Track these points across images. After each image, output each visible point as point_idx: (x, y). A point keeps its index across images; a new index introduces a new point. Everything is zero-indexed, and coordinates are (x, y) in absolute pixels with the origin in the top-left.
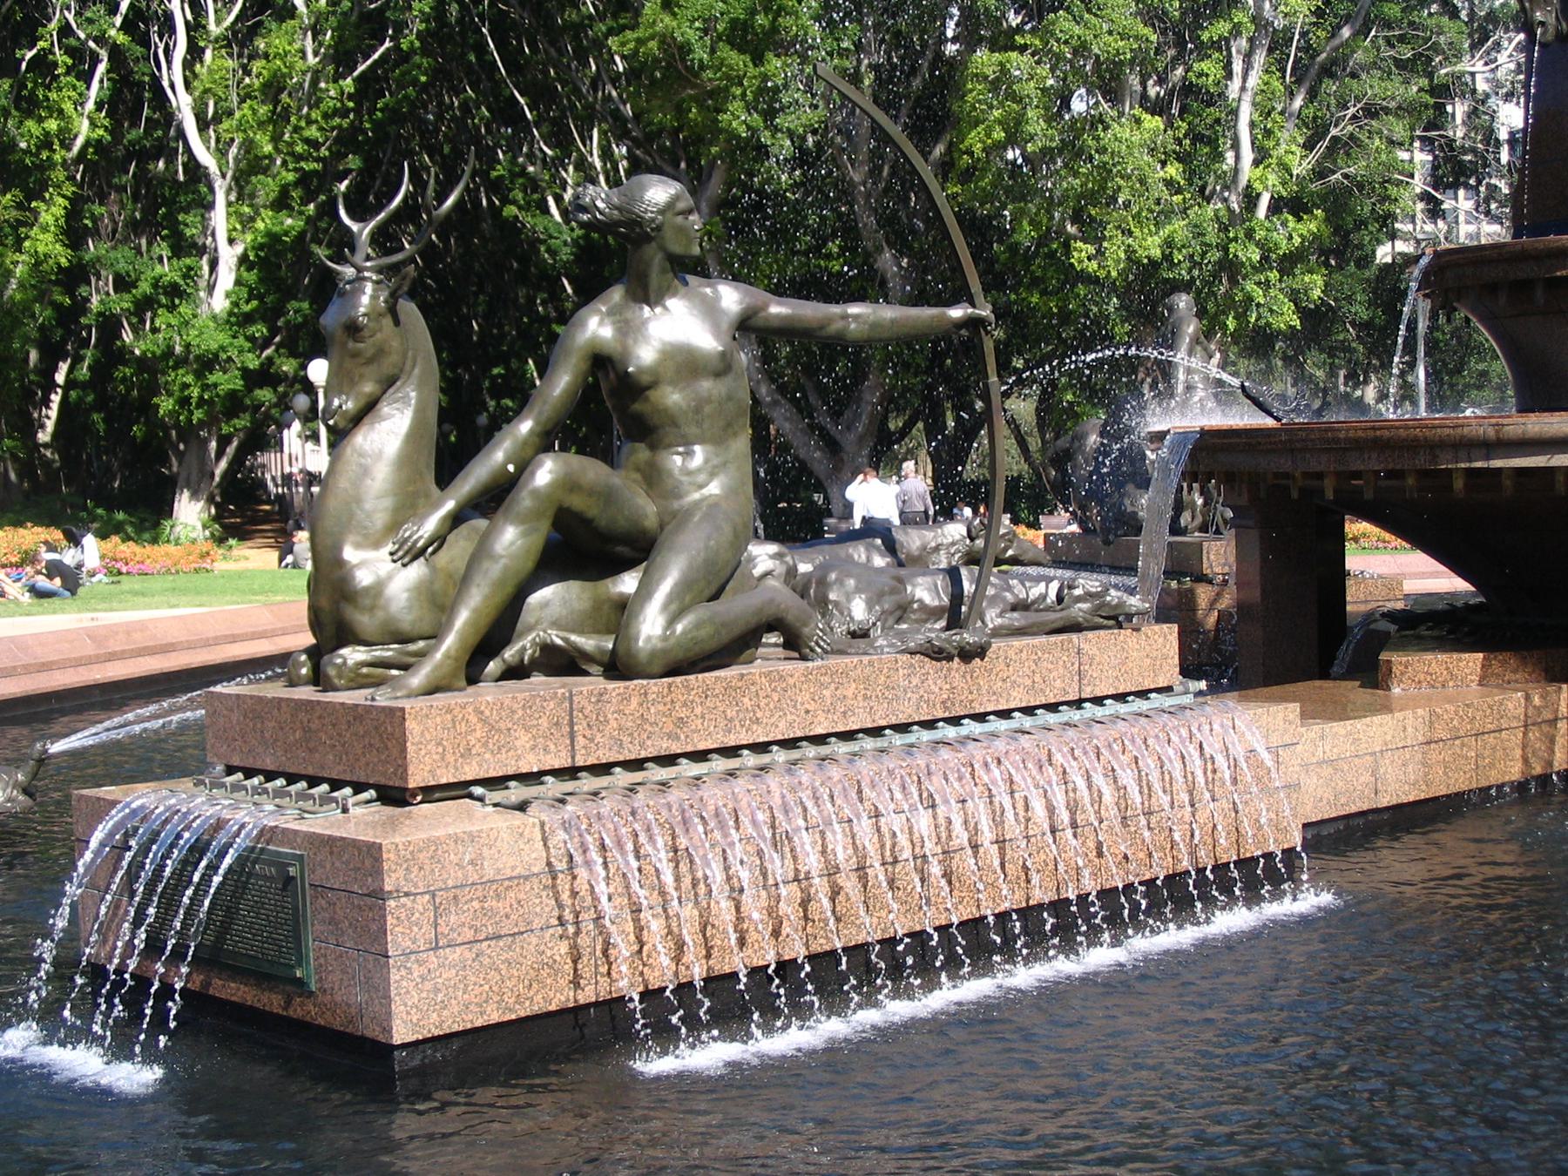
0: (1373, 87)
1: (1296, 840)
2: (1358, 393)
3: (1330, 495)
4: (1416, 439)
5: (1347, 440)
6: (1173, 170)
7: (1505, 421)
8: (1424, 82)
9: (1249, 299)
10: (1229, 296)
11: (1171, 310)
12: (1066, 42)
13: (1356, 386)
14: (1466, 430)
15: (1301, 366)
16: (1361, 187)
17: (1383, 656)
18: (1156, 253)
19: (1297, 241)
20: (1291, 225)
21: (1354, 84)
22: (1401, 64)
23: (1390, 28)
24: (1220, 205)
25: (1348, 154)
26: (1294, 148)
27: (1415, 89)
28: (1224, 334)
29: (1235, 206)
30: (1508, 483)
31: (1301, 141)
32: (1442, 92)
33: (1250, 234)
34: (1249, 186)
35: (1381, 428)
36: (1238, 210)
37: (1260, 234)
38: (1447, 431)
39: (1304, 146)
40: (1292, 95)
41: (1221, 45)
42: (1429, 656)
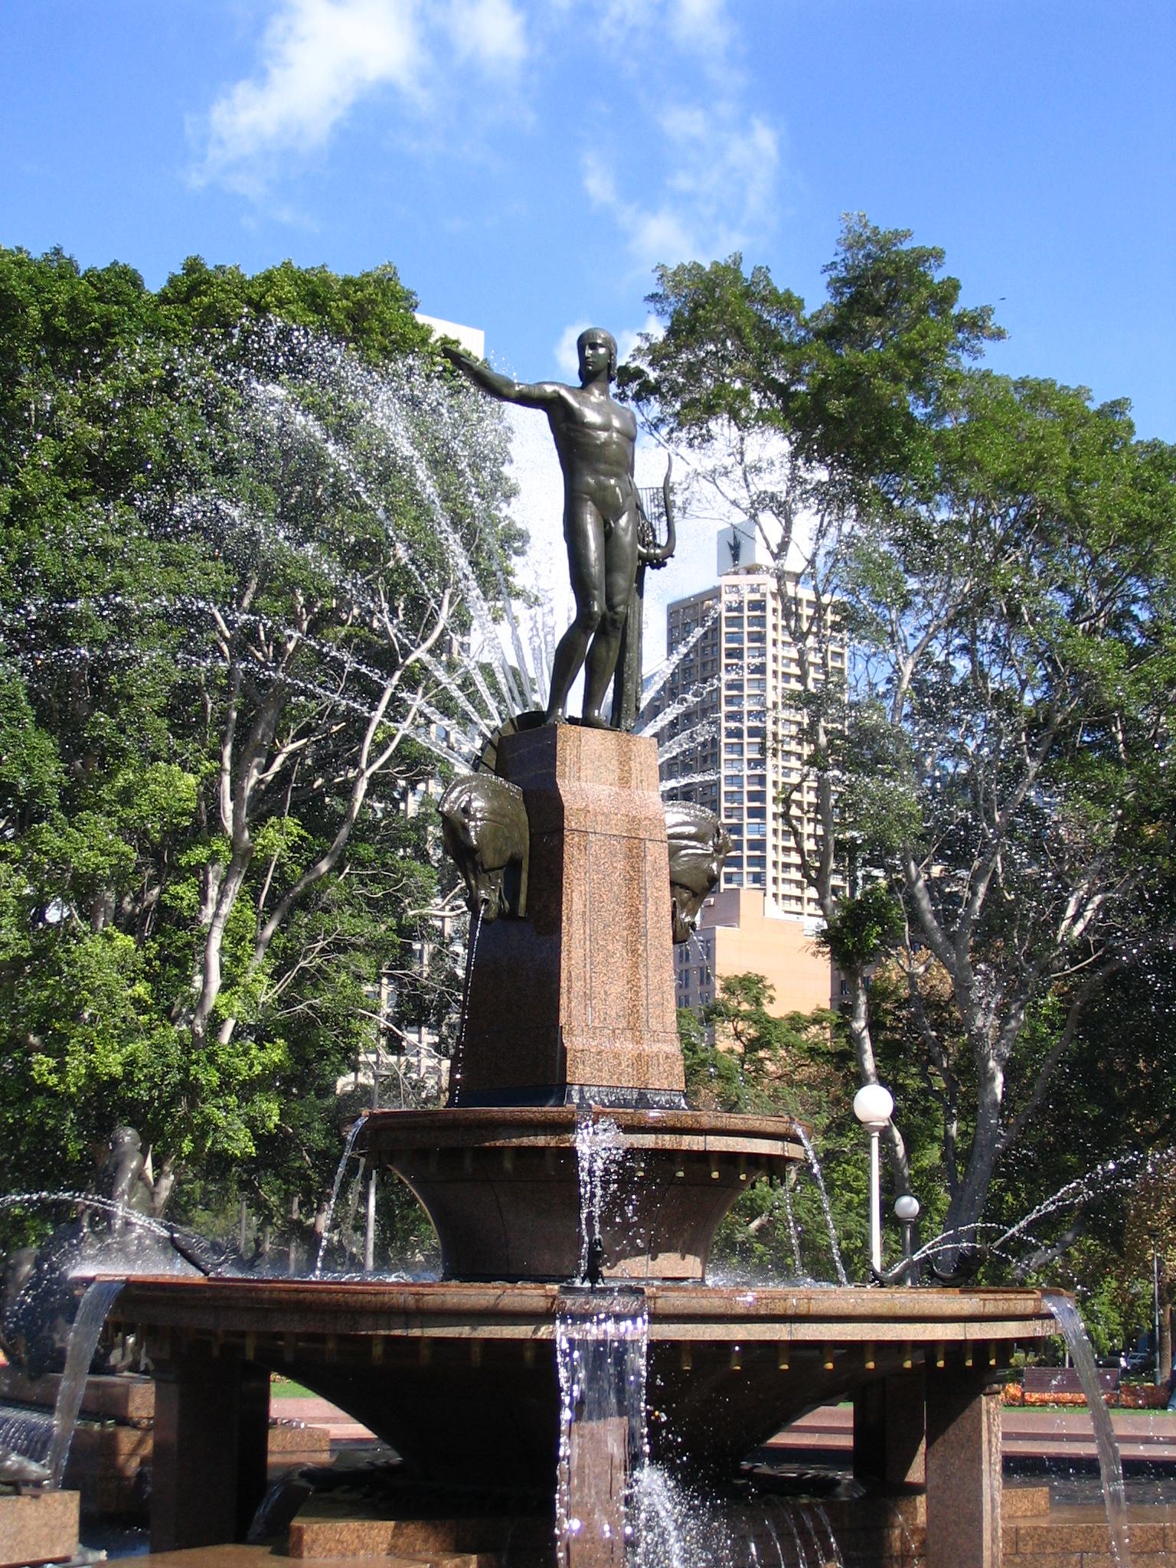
0: (344, 923)
1: (839, 1013)
2: (312, 1220)
3: (250, 1355)
4: (338, 1304)
5: (271, 1301)
6: (141, 989)
7: (427, 1290)
8: (392, 921)
9: (208, 1121)
10: (185, 1119)
11: (115, 1144)
12: (46, 853)
13: (308, 1216)
14: (386, 1298)
15: (255, 1191)
16: (325, 1018)
17: (296, 1522)
18: (118, 1071)
19: (258, 1069)
20: (254, 1052)
21: (326, 918)
22: (371, 903)
23: (365, 868)
24: (184, 1027)
25: (315, 986)
26: (261, 977)
27: (383, 927)
28: (179, 1157)
29: (200, 1029)
30: (426, 1352)
31: (269, 971)
32: (406, 932)
33: (211, 1058)
34: (214, 1011)
35: (304, 1291)
36: (202, 1034)
37: (222, 1058)
38: (369, 1298)
39: (271, 976)
40: (264, 924)
41: (198, 870)
42: (341, 1524)
